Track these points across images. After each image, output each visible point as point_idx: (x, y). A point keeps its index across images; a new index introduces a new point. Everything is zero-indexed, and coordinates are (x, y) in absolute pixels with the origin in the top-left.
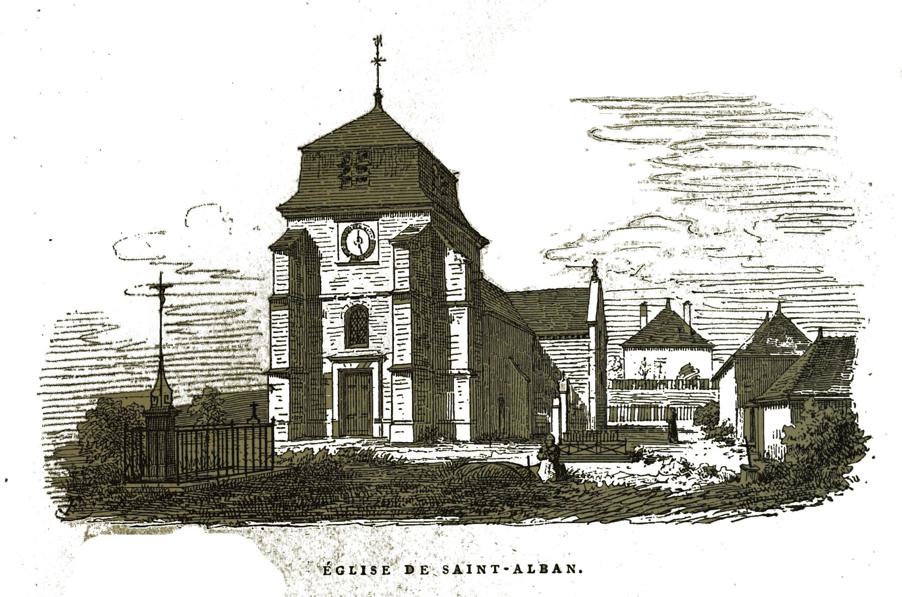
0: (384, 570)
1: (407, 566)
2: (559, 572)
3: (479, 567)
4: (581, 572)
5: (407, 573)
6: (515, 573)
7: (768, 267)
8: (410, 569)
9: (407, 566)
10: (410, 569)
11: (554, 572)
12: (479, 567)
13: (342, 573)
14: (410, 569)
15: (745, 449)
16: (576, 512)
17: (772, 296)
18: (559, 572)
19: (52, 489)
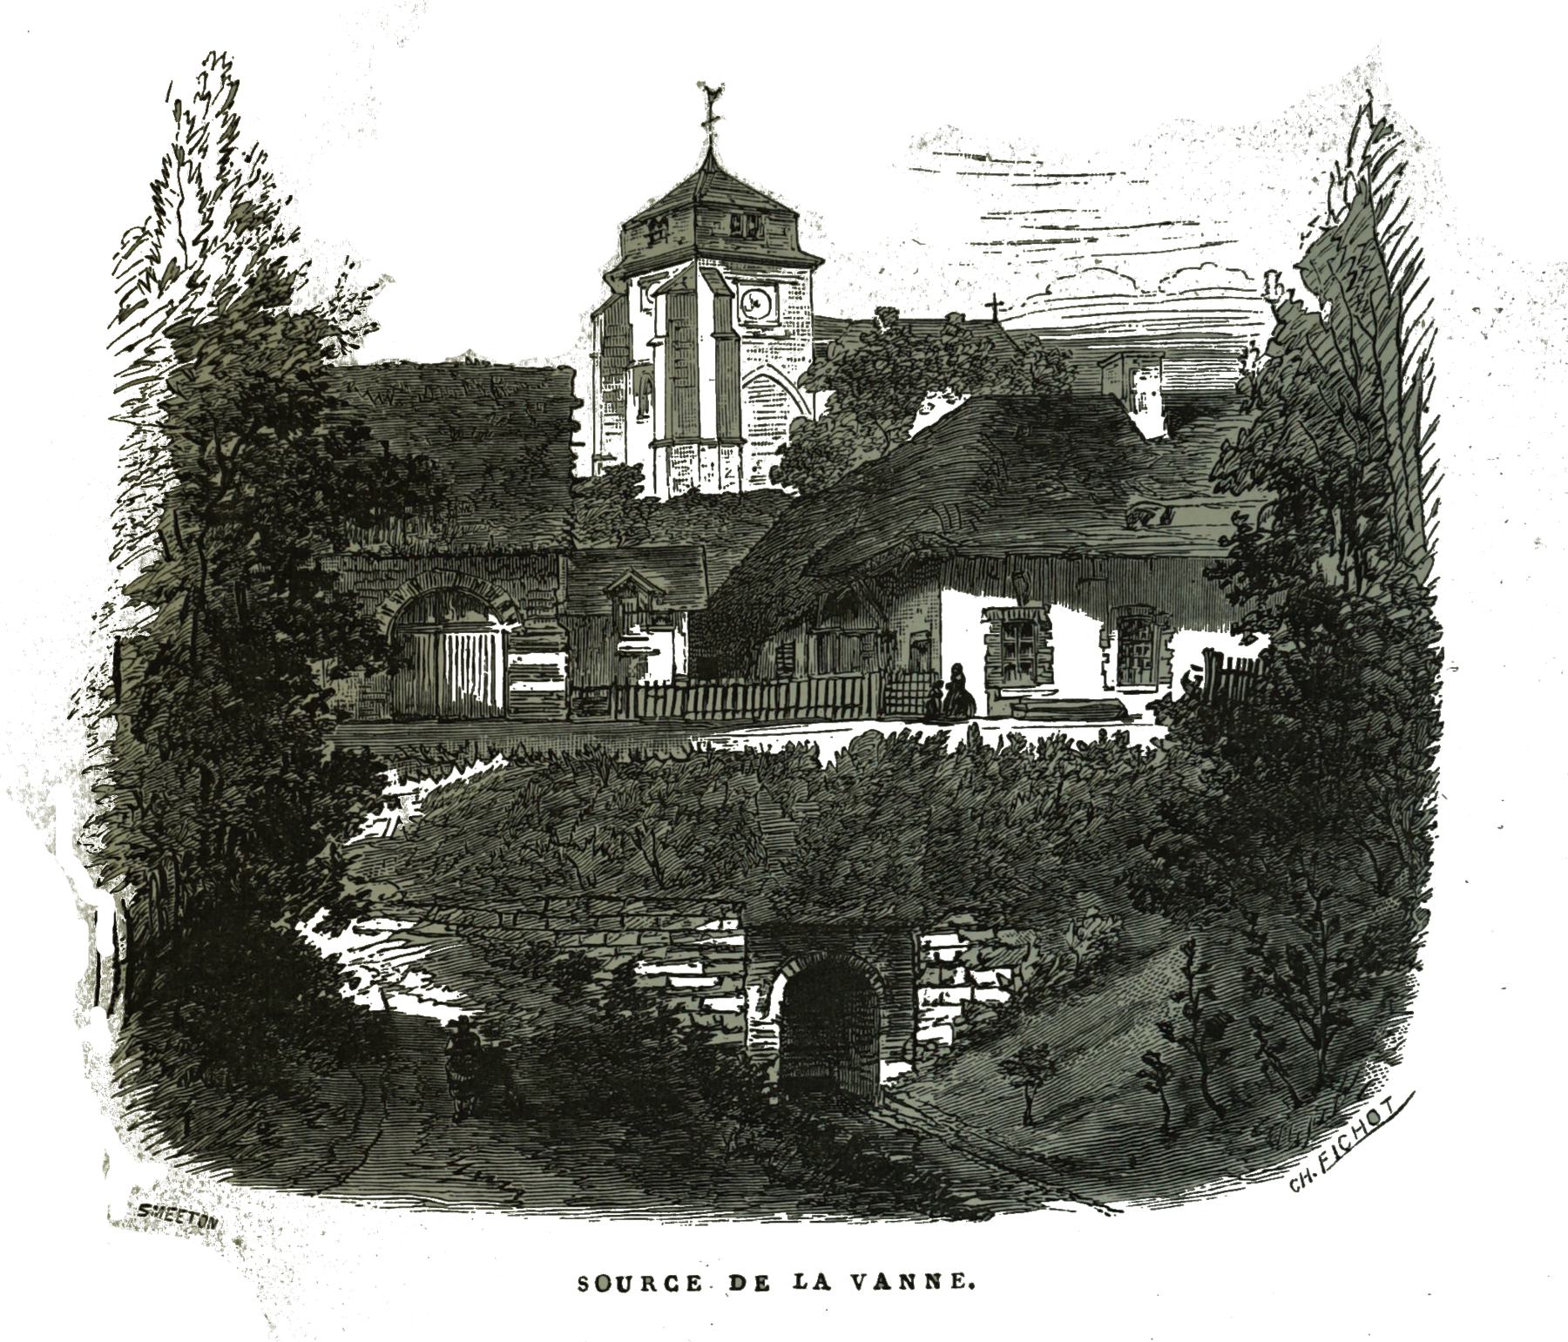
0: (955, 1280)
1: (734, 1277)
2: (887, 1287)
3: (929, 1276)
4: (972, 1286)
5: (734, 1288)
6: (876, 1288)
7: (994, 243)
8: (738, 1282)
9: (734, 1277)
10: (737, 1282)
11: (816, 1288)
12: (903, 1277)
13: (676, 1289)
14: (738, 1282)
15: (985, 906)
16: (234, 1162)
17: (1356, 242)
18: (887, 1287)
19: (186, 1158)
